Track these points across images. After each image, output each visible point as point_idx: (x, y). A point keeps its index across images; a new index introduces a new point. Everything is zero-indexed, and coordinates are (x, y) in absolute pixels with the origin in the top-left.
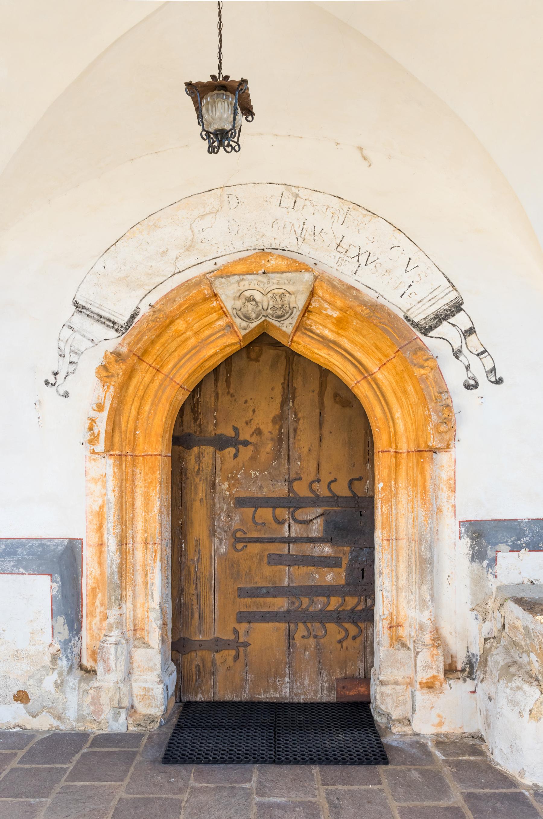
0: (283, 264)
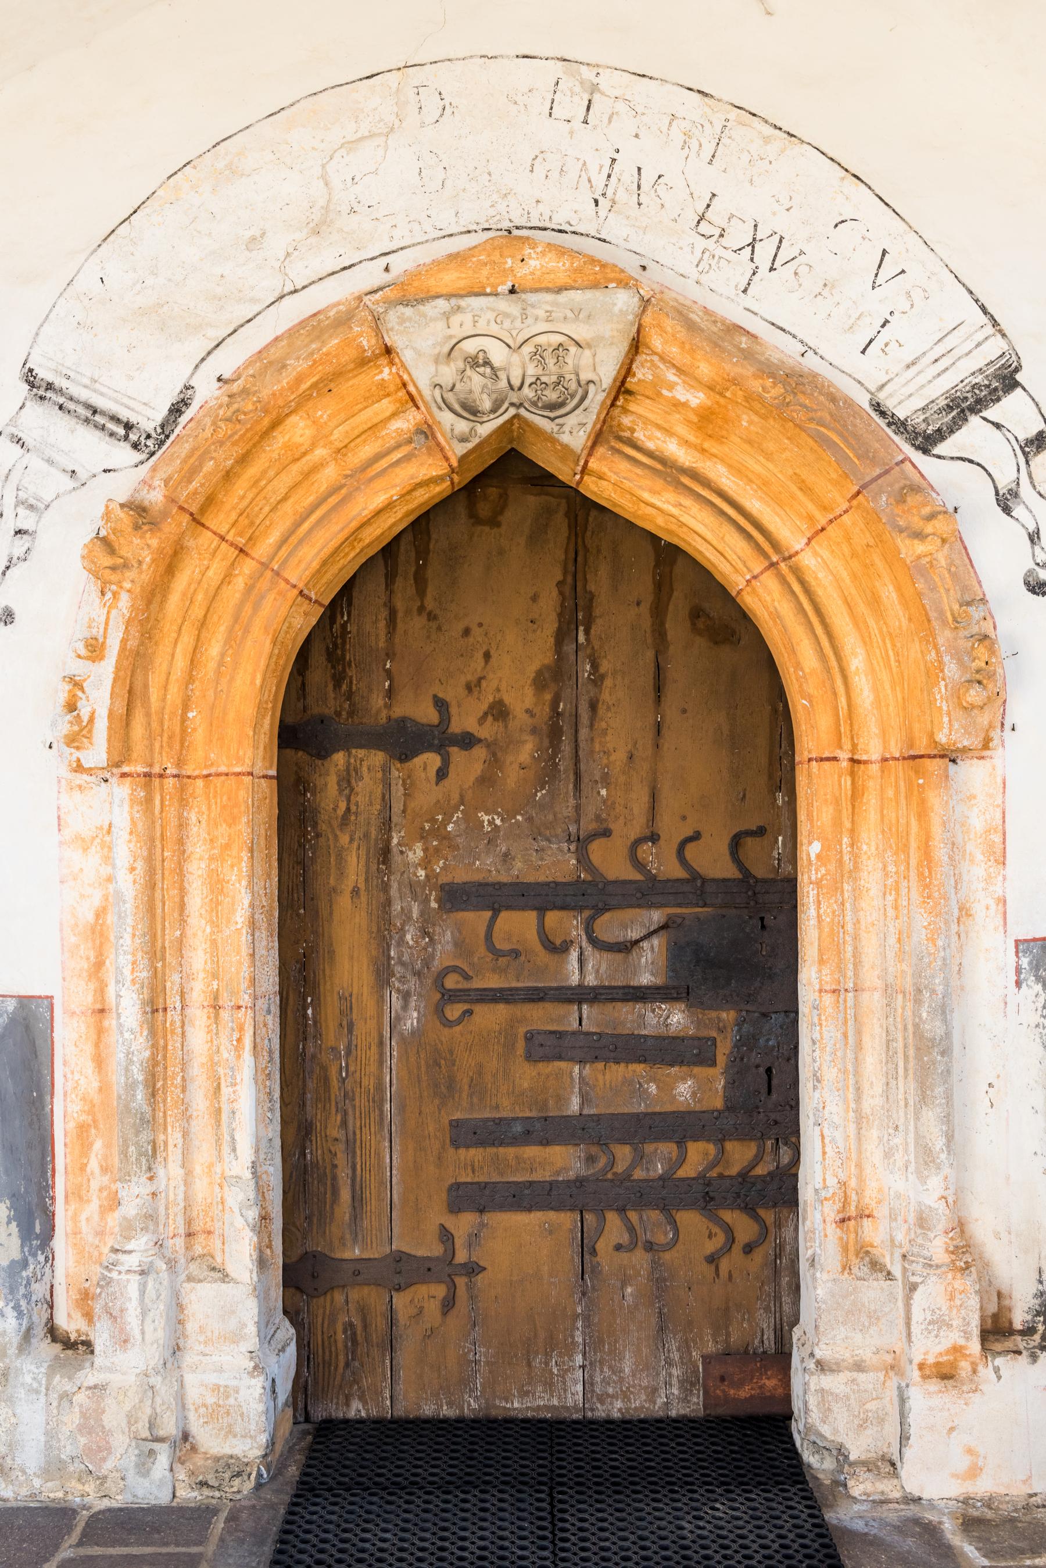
0: (560, 268)
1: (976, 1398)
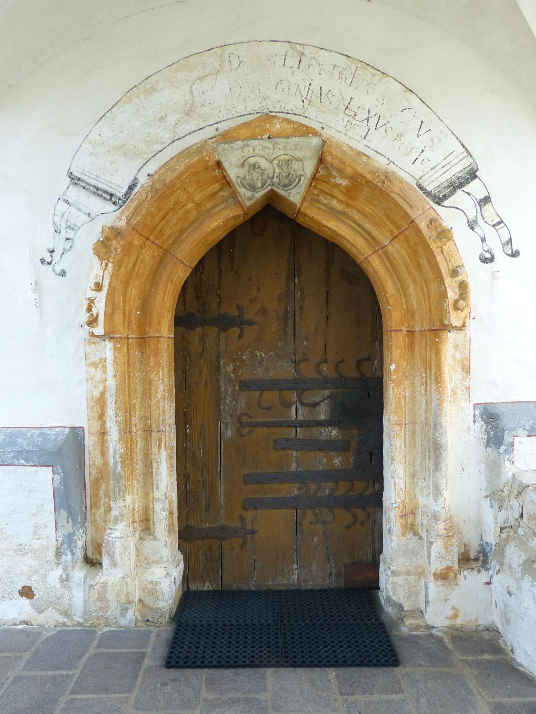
1: (457, 588)
